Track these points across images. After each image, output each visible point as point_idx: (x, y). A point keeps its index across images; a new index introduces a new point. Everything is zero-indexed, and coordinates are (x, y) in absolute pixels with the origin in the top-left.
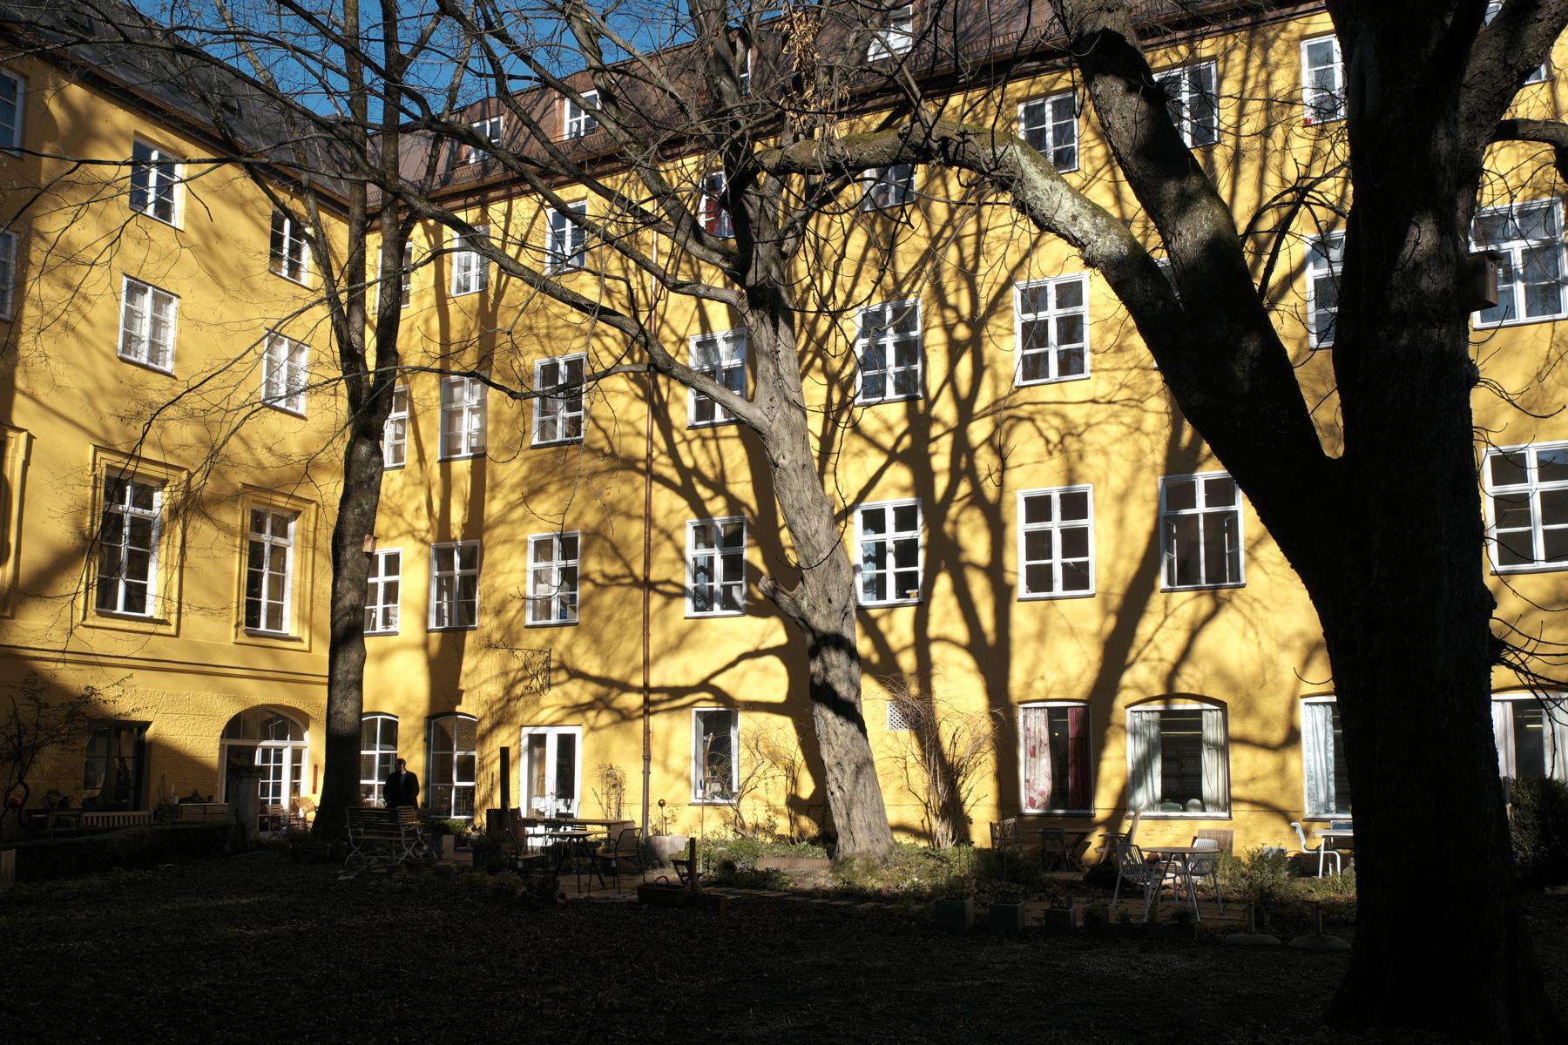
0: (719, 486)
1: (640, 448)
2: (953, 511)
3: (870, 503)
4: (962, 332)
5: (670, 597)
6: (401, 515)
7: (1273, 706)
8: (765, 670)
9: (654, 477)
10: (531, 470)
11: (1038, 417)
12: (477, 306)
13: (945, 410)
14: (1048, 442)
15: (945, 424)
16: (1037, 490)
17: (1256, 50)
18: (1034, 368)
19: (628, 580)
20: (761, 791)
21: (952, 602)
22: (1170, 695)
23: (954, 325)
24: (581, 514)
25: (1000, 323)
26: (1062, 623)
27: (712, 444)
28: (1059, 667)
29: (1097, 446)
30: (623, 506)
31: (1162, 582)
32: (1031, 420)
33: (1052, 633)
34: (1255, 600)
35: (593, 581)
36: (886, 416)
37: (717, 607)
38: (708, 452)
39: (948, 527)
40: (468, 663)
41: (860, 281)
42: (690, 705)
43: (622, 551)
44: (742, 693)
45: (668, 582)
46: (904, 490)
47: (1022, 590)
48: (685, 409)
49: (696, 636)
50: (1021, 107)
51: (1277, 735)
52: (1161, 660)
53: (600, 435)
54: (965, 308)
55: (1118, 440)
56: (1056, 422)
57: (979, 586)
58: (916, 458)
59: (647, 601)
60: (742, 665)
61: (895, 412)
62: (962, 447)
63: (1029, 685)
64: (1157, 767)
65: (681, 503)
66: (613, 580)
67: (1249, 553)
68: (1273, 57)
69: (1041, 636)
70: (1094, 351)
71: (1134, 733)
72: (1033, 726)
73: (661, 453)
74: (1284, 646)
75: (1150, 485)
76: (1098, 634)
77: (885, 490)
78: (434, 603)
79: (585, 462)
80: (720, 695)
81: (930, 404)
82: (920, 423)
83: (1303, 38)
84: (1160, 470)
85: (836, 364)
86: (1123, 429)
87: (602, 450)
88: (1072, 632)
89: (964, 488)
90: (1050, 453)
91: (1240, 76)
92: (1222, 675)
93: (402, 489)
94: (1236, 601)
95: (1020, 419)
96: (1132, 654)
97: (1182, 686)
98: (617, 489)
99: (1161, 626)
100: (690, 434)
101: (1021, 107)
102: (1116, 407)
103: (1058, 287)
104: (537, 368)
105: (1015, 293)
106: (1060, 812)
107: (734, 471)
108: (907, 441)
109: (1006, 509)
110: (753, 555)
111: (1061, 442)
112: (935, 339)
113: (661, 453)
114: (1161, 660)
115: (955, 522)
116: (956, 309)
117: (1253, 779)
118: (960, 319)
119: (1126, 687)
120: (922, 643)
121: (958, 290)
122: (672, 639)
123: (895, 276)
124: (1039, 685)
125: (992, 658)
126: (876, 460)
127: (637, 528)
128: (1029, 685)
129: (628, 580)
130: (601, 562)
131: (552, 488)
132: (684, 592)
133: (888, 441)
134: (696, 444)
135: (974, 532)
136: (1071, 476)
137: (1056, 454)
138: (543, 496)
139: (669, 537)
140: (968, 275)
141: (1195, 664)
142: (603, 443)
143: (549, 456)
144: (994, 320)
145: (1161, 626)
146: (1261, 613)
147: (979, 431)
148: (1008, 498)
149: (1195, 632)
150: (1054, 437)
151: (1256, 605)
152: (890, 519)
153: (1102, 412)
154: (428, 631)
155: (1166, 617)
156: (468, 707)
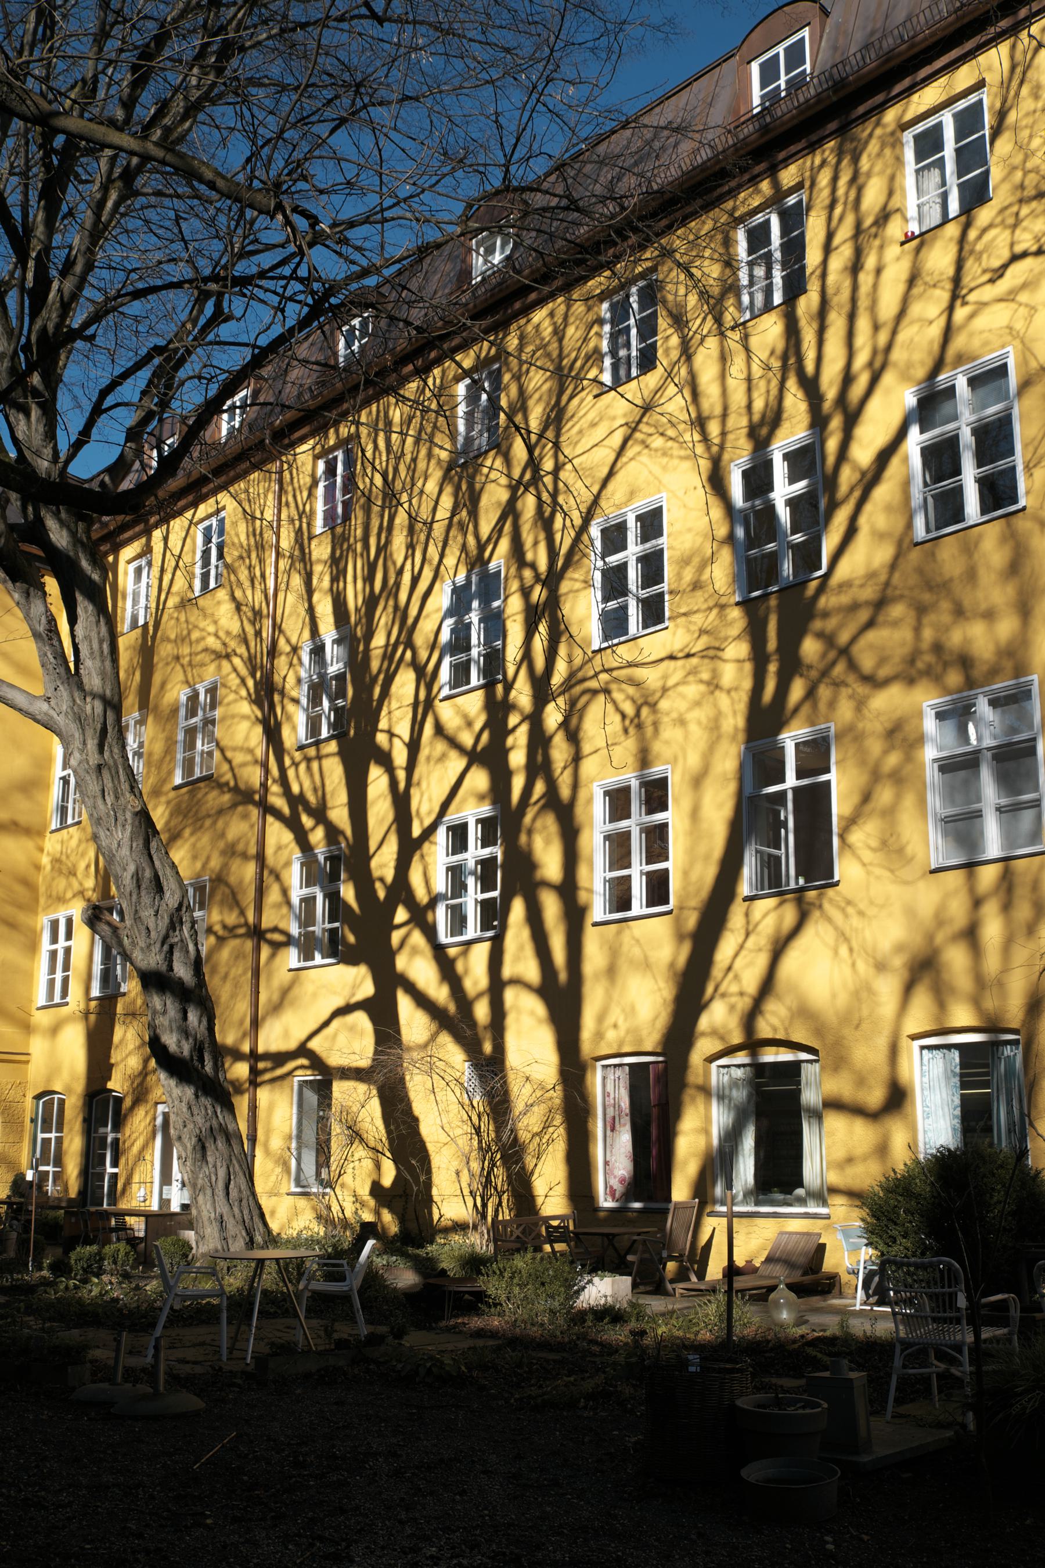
0: (320, 814)
1: (253, 776)
2: (528, 819)
3: (452, 817)
4: (538, 594)
5: (276, 946)
6: (75, 875)
7: (869, 1054)
8: (352, 1029)
9: (268, 809)
10: (171, 815)
11: (613, 687)
12: (140, 641)
13: (522, 695)
14: (624, 716)
15: (522, 713)
16: (614, 779)
17: (845, 162)
18: (614, 625)
19: (242, 931)
20: (347, 1178)
21: (526, 933)
22: (753, 1044)
23: (532, 587)
24: (208, 859)
25: (576, 576)
26: (636, 951)
27: (315, 765)
28: (631, 1011)
29: (674, 715)
30: (240, 847)
31: (745, 888)
32: (607, 691)
33: (623, 966)
34: (849, 903)
35: (215, 934)
36: (463, 710)
37: (318, 956)
38: (311, 775)
39: (523, 839)
40: (118, 1033)
41: (447, 551)
42: (290, 1074)
43: (239, 897)
44: (334, 1060)
45: (275, 929)
46: (481, 798)
47: (598, 910)
48: (294, 728)
49: (295, 991)
50: (605, 306)
51: (875, 1097)
52: (742, 994)
53: (226, 767)
54: (543, 565)
55: (698, 704)
56: (631, 690)
57: (551, 906)
58: (490, 756)
59: (257, 950)
60: (335, 1023)
61: (473, 703)
62: (539, 741)
63: (599, 1035)
64: (748, 1142)
65: (288, 837)
66: (230, 930)
67: (841, 837)
68: (865, 163)
69: (611, 971)
70: (671, 592)
71: (721, 1098)
72: (608, 1089)
73: (274, 781)
74: (881, 967)
75: (728, 760)
76: (672, 965)
77: (464, 800)
78: (97, 968)
79: (215, 799)
80: (317, 1063)
81: (509, 687)
82: (497, 710)
83: (904, 127)
84: (741, 737)
85: (423, 655)
86: (702, 688)
87: (227, 784)
88: (646, 965)
89: (539, 788)
90: (626, 731)
91: (827, 202)
92: (804, 1012)
93: (78, 846)
94: (826, 905)
95: (595, 692)
96: (710, 990)
97: (764, 1029)
98: (240, 827)
99: (742, 947)
100: (298, 756)
101: (605, 306)
102: (694, 661)
103: (638, 518)
104: (183, 699)
105: (595, 531)
106: (637, 1205)
107: (333, 793)
108: (485, 737)
109: (579, 810)
110: (348, 892)
111: (638, 714)
112: (514, 606)
113: (274, 781)
114: (742, 994)
115: (530, 832)
116: (533, 566)
117: (850, 1160)
118: (537, 577)
119: (703, 1034)
120: (497, 986)
121: (536, 543)
122: (276, 997)
123: (477, 536)
124: (611, 1035)
125: (563, 1000)
126: (457, 763)
127: (250, 870)
128: (599, 1035)
129: (242, 931)
130: (221, 913)
131: (187, 832)
132: (290, 941)
133: (467, 739)
134: (303, 767)
135: (547, 842)
136: (644, 759)
137: (632, 731)
138: (179, 842)
139: (278, 878)
140: (545, 522)
141: (779, 998)
142: (229, 777)
143: (186, 797)
144: (570, 574)
145: (742, 947)
146: (855, 921)
147: (553, 716)
148: (582, 794)
149: (779, 948)
150: (629, 709)
151: (850, 910)
152: (474, 833)
153: (676, 670)
154: (90, 1000)
155: (748, 934)
156: (117, 1084)
